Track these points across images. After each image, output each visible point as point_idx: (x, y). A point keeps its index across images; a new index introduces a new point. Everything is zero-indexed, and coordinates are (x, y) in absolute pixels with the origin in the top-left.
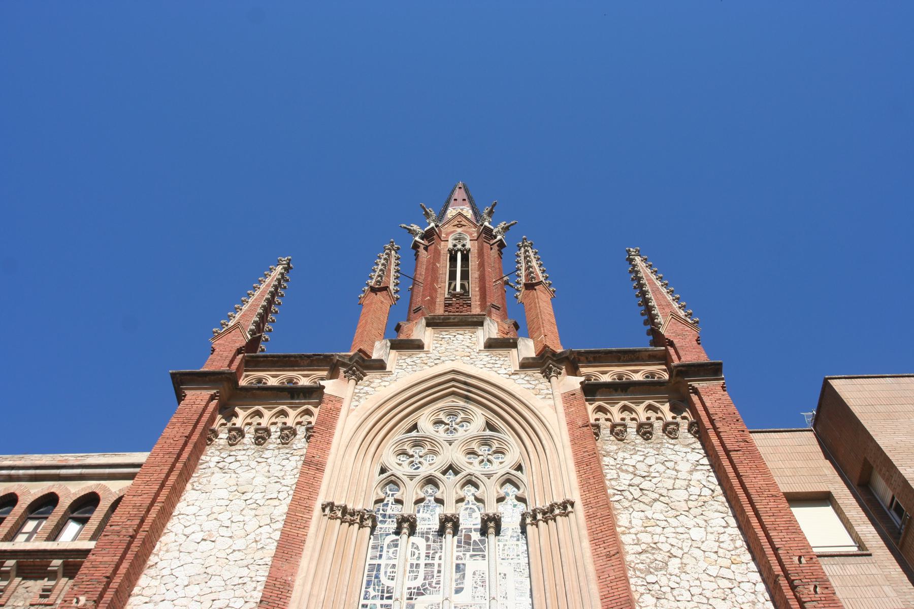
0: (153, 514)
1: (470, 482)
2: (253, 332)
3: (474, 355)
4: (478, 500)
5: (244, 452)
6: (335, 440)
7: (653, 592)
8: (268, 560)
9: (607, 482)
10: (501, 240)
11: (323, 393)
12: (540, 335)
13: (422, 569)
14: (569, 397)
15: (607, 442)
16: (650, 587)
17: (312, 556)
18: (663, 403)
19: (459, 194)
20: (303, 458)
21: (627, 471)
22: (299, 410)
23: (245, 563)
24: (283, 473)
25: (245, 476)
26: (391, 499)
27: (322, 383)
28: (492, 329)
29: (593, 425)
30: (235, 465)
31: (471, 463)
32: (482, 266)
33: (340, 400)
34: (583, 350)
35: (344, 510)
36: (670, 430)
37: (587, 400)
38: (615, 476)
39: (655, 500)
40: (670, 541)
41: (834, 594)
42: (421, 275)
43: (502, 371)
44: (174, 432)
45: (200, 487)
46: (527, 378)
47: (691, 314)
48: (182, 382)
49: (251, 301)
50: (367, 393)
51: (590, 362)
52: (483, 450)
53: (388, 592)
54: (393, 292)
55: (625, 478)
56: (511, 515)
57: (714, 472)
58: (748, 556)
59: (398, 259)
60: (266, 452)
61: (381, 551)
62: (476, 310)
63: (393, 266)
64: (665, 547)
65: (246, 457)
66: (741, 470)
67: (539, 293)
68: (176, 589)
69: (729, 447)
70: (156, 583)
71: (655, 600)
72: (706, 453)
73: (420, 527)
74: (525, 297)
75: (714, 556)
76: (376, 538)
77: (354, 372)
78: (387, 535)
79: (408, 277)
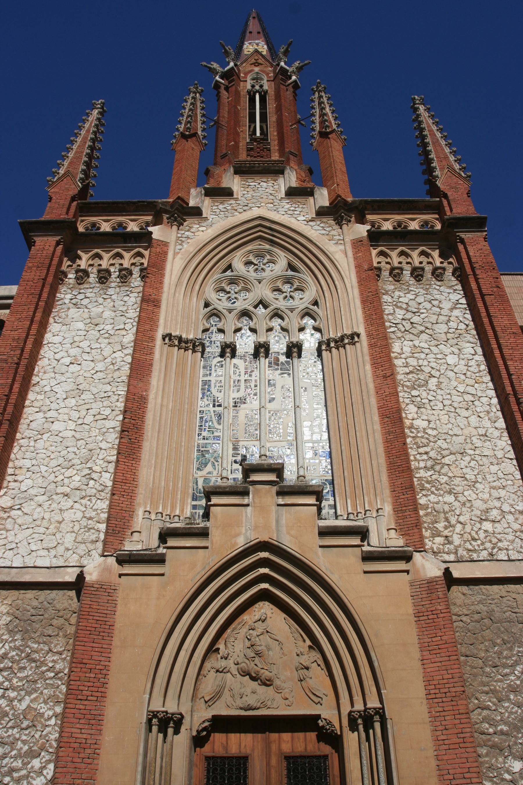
0: (29, 345)
1: (277, 314)
2: (82, 180)
3: (276, 202)
4: (283, 329)
5: (91, 290)
6: (166, 280)
7: (415, 403)
8: (125, 378)
9: (385, 317)
10: (295, 81)
11: (151, 238)
13: (242, 384)
14: (357, 244)
15: (387, 284)
16: (413, 399)
18: (434, 250)
19: (253, 25)
20: (141, 295)
21: (401, 308)
22: (133, 252)
23: (107, 381)
24: (126, 308)
25: (96, 310)
26: (214, 329)
27: (150, 229)
28: (292, 178)
29: (376, 268)
30: (85, 302)
31: (277, 299)
32: (279, 109)
33: (166, 244)
35: (180, 339)
36: (438, 274)
37: (371, 246)
38: (392, 312)
39: (422, 332)
40: (431, 364)
42: (223, 117)
43: (301, 218)
44: (32, 274)
45: (61, 320)
46: (322, 225)
47: (464, 168)
48: (31, 230)
49: (75, 147)
51: (375, 210)
52: (286, 288)
54: (201, 137)
55: (400, 314)
56: (310, 340)
57: (470, 310)
58: (488, 378)
60: (110, 290)
61: (211, 370)
62: (275, 156)
63: (199, 111)
64: (427, 369)
66: (492, 311)
67: (333, 142)
68: (58, 401)
69: (484, 291)
70: (42, 397)
71: (416, 409)
72: (464, 294)
73: (240, 350)
75: (463, 377)
76: (206, 360)
79: (214, 126)
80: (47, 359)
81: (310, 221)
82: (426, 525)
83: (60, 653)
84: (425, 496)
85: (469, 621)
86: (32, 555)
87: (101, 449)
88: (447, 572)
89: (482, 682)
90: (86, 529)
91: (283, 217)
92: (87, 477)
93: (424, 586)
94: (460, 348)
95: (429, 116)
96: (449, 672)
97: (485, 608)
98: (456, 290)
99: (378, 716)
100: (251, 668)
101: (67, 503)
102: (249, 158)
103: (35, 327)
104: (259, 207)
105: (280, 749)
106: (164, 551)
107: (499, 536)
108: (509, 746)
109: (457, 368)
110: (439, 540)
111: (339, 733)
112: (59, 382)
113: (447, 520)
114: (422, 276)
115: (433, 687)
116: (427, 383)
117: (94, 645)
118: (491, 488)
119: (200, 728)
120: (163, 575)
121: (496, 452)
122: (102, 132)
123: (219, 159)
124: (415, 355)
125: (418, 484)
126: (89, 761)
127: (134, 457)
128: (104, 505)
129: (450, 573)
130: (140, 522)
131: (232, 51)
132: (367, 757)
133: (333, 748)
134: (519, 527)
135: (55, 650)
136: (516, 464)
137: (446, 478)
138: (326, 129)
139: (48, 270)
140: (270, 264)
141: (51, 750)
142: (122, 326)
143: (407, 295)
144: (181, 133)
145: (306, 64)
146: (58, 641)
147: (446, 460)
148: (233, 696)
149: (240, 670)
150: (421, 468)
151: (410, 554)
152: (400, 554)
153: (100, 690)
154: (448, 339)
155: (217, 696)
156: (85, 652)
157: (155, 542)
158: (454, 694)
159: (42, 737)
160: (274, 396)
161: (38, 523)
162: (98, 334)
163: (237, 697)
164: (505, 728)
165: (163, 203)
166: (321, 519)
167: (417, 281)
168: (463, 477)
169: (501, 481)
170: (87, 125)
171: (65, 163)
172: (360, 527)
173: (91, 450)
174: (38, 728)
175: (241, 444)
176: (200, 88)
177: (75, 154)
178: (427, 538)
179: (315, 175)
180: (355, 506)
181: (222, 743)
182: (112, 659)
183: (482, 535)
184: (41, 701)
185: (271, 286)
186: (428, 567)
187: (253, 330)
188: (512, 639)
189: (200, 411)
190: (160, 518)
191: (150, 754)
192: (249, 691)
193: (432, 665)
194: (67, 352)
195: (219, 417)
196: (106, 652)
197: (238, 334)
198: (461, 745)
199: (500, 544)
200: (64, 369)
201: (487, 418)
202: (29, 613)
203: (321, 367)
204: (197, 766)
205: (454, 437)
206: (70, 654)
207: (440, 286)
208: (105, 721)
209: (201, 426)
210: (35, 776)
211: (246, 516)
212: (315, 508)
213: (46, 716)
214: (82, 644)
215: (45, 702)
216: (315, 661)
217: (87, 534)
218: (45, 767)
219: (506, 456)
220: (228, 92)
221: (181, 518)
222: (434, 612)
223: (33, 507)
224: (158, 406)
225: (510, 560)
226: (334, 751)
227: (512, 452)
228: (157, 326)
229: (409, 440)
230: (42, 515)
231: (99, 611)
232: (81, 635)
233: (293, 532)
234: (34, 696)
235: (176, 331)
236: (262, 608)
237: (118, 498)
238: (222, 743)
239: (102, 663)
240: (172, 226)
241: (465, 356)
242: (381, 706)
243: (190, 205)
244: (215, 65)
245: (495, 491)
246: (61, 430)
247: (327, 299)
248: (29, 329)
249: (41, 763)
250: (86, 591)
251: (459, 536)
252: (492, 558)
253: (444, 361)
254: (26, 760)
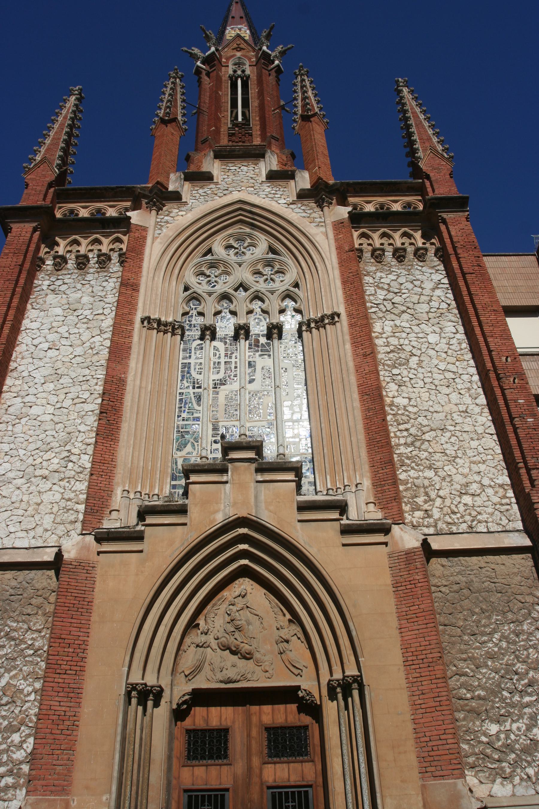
1: (257, 297)
2: (59, 166)
5: (69, 276)
6: (145, 265)
8: (103, 362)
9: (367, 297)
10: (278, 66)
11: (130, 223)
13: (222, 366)
14: (338, 225)
15: (369, 265)
17: (138, 359)
18: (416, 231)
19: (236, 10)
20: (120, 280)
21: (382, 288)
22: (111, 238)
23: (85, 365)
24: (104, 293)
26: (194, 312)
27: (128, 214)
28: (272, 162)
29: (357, 250)
31: (257, 282)
32: (261, 94)
35: (159, 322)
36: (420, 255)
37: (353, 228)
38: (373, 292)
39: (403, 312)
40: (412, 343)
41: (527, 383)
42: (205, 103)
43: (282, 201)
45: (38, 306)
46: (303, 208)
47: (447, 149)
49: (52, 134)
51: (357, 192)
52: (267, 271)
53: (198, 383)
54: (181, 122)
55: (381, 294)
56: (290, 322)
57: (452, 289)
58: (470, 356)
60: (88, 275)
61: (190, 353)
62: (257, 141)
63: (179, 96)
64: (408, 348)
65: (71, 281)
66: (473, 289)
67: (315, 125)
68: (36, 386)
69: (465, 270)
70: (20, 382)
71: (397, 387)
72: (447, 274)
73: (220, 333)
75: (444, 355)
76: (185, 343)
80: (25, 345)
81: (291, 204)
82: (405, 500)
83: (40, 631)
84: (405, 471)
85: (448, 591)
86: (11, 536)
87: (79, 431)
88: (425, 544)
89: (461, 650)
90: (65, 510)
91: (264, 200)
92: (66, 459)
93: (402, 557)
94: (441, 326)
95: (413, 99)
96: (426, 639)
97: (464, 579)
98: (438, 270)
99: (356, 684)
100: (231, 642)
101: (45, 486)
102: (230, 143)
103: (12, 312)
104: (239, 191)
105: (260, 721)
106: (143, 528)
107: (478, 509)
108: (486, 710)
109: (438, 346)
110: (418, 514)
111: (319, 703)
112: (37, 367)
113: (427, 494)
114: (404, 257)
115: (411, 654)
116: (408, 361)
117: (73, 621)
118: (471, 462)
119: (181, 701)
120: (141, 551)
121: (476, 428)
122: (80, 119)
124: (396, 334)
125: (398, 460)
126: (69, 732)
127: (113, 438)
128: (83, 486)
129: (429, 545)
130: (118, 501)
131: (213, 35)
132: (345, 724)
133: (313, 719)
134: (499, 500)
135: (34, 629)
136: (497, 439)
137: (426, 454)
139: (25, 256)
140: (251, 247)
141: (30, 725)
142: (101, 311)
143: (389, 276)
144: (161, 118)
145: (289, 49)
146: (37, 619)
147: (427, 437)
148: (213, 670)
149: (220, 645)
150: (402, 445)
151: (388, 527)
152: (378, 527)
153: (79, 664)
154: (430, 319)
155: (197, 669)
156: (64, 628)
157: (133, 519)
158: (431, 660)
159: (22, 712)
160: (254, 378)
161: (17, 505)
162: (77, 319)
163: (217, 670)
164: (482, 693)
165: (142, 188)
166: (301, 495)
167: (398, 261)
168: (444, 453)
169: (481, 456)
170: (64, 112)
171: (41, 150)
172: (338, 501)
173: (69, 433)
174: (18, 704)
175: (221, 424)
176: (180, 73)
177: (52, 140)
178: (406, 512)
180: (334, 482)
181: (203, 717)
182: (90, 635)
183: (461, 508)
184: (21, 678)
185: (251, 269)
186: (407, 538)
187: (234, 313)
188: (490, 607)
189: (180, 393)
190: (139, 496)
191: (130, 726)
192: (229, 664)
193: (409, 633)
194: (45, 337)
195: (199, 398)
196: (85, 627)
197: (219, 317)
198: (438, 708)
199: (479, 517)
200: (42, 354)
201: (467, 395)
202: (8, 593)
203: (301, 348)
204: (177, 739)
205: (435, 414)
206: (49, 632)
207: (422, 267)
208: (84, 694)
209: (181, 407)
210: (14, 750)
211: (225, 493)
212: (294, 483)
213: (25, 692)
214: (61, 619)
215: (25, 679)
216: (295, 634)
217: (66, 515)
218: (24, 741)
219: (487, 431)
220: (209, 77)
221: (160, 496)
222: (412, 582)
223: (11, 490)
224: (137, 388)
225: (489, 532)
226: (314, 722)
227: (493, 427)
228: (136, 310)
229: (389, 418)
230: (20, 497)
231: (77, 588)
232: (59, 611)
233: (272, 508)
234: (14, 673)
235: (154, 314)
236: (242, 584)
237: (96, 478)
238: (203, 717)
239: (81, 638)
240: (151, 210)
241: (447, 335)
242: (359, 674)
244: (196, 51)
245: (475, 465)
246: (39, 414)
247: (308, 281)
248: (6, 315)
249: (21, 737)
250: (64, 569)
251: (439, 510)
252: (471, 530)
253: (425, 340)
254: (5, 735)
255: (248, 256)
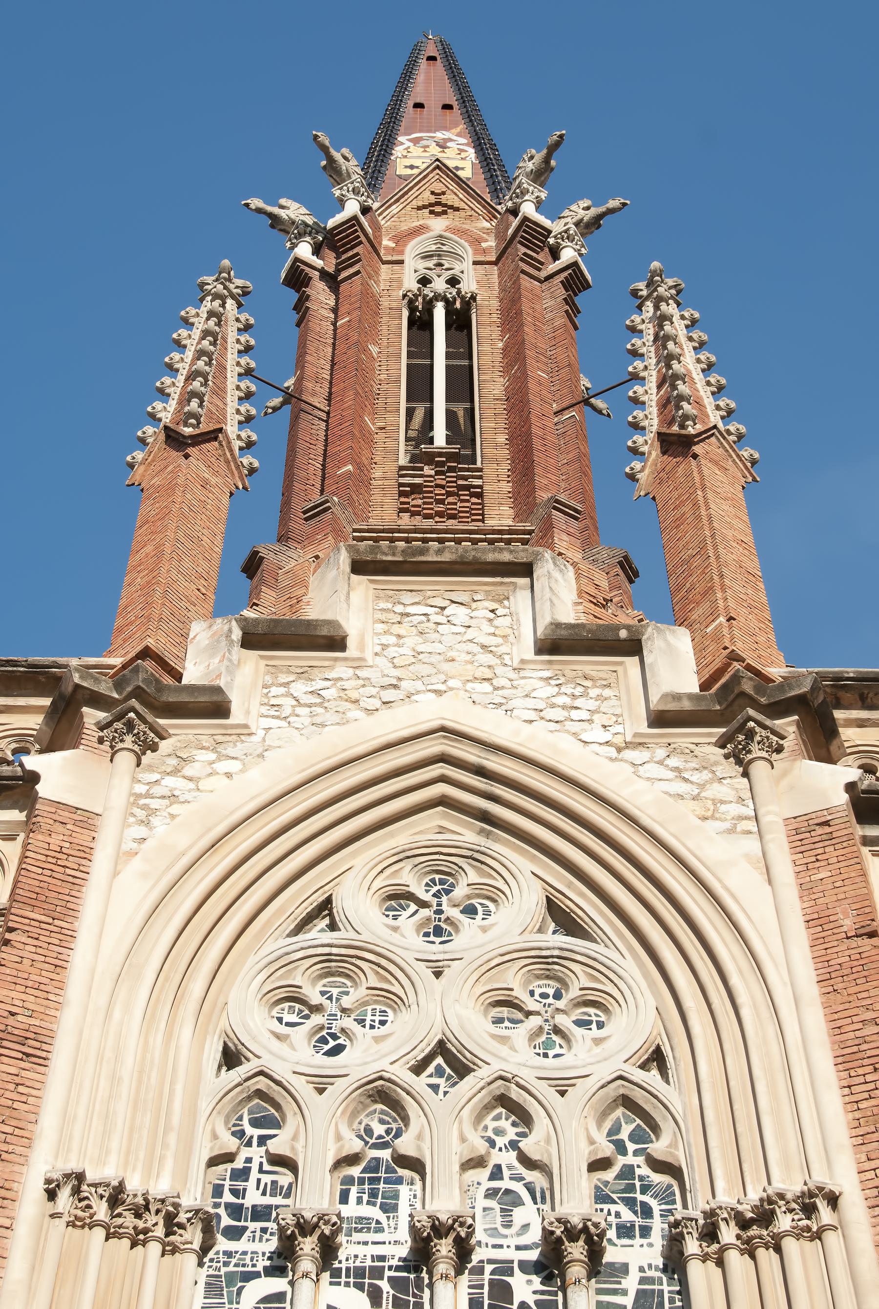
6: (82, 957)
12: (713, 615)
14: (810, 834)
19: (430, 84)
27: (32, 762)
28: (560, 592)
32: (515, 356)
33: (86, 820)
34: (851, 671)
35: (116, 1196)
46: (673, 762)
50: (172, 797)
54: (237, 444)
59: (247, 328)
62: (479, 465)
63: (231, 357)
73: (352, 1251)
74: (661, 477)
77: (130, 726)
78: (248, 1277)
81: (628, 745)
102: (405, 520)
123: (297, 524)
131: (353, 162)
138: (682, 426)
144: (166, 428)
176: (239, 282)
179: (648, 580)
235: (150, 1170)
243: (185, 681)
255: (470, 936)
